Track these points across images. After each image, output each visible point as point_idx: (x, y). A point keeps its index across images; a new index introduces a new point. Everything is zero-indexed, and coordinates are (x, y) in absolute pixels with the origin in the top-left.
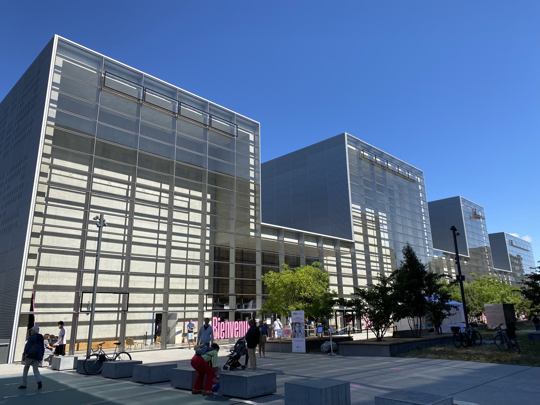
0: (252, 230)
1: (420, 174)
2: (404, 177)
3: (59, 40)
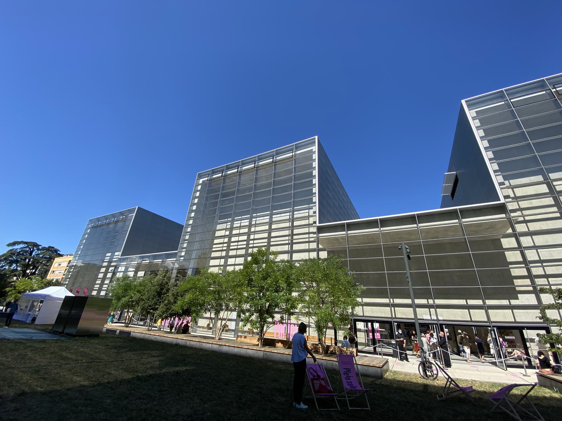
3: (466, 102)
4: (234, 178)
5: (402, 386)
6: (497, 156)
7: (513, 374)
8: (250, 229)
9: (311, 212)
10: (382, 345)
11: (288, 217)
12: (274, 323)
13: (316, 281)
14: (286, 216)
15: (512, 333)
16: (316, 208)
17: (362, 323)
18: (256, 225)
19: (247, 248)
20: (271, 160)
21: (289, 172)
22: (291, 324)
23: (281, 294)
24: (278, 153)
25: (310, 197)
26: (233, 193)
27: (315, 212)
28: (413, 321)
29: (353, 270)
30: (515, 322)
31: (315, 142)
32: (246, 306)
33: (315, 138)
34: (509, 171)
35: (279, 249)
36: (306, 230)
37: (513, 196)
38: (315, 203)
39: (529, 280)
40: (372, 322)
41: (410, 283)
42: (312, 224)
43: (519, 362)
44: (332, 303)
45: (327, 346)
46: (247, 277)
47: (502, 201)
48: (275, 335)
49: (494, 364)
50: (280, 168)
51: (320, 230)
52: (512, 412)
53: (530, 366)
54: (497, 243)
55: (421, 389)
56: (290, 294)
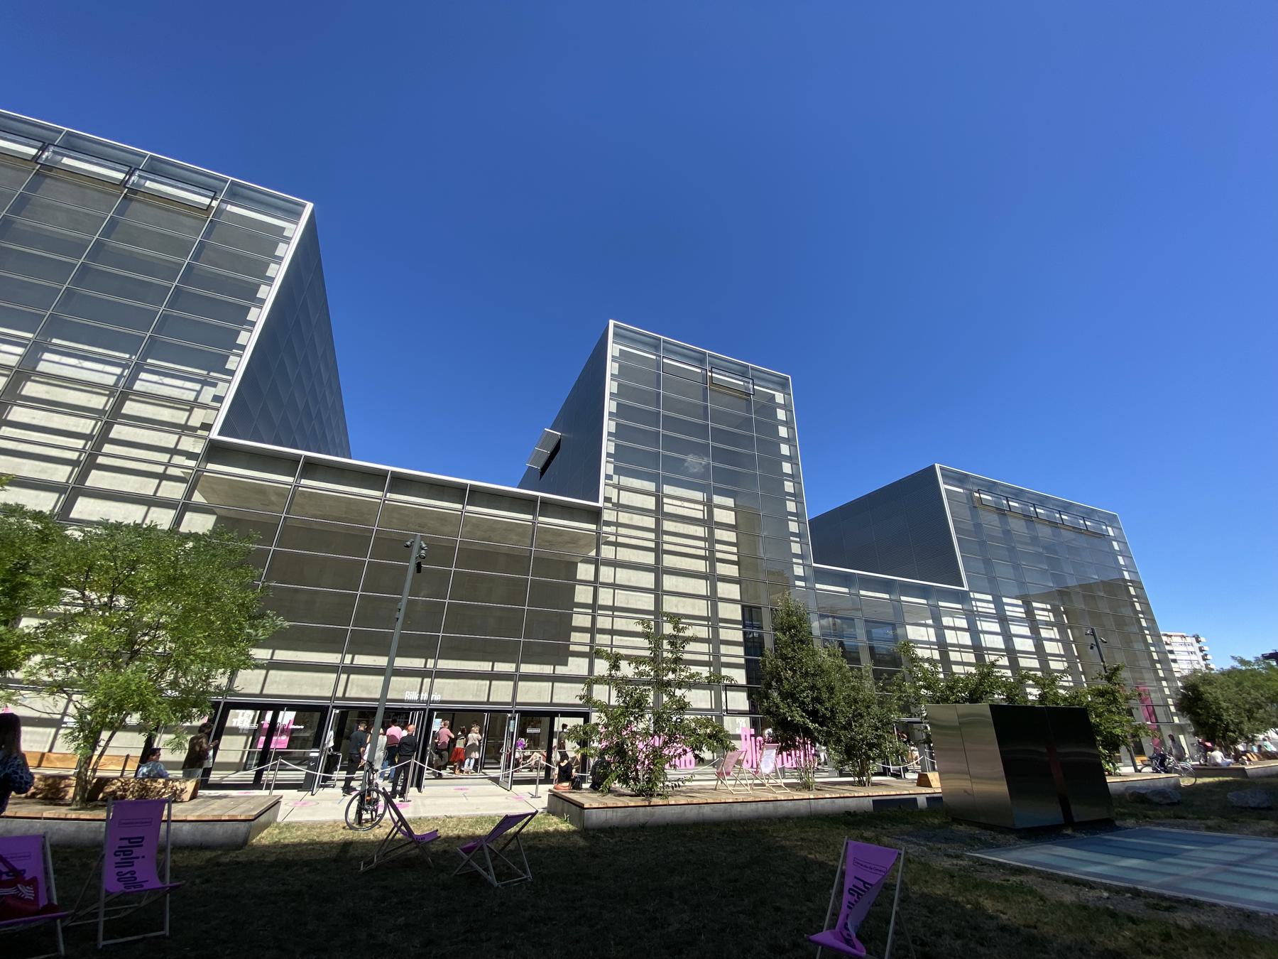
0: (799, 578)
1: (1112, 520)
2: (1076, 530)
3: (615, 326)
5: (290, 856)
6: (619, 433)
9: (208, 394)
10: (282, 764)
11: (110, 380)
13: (130, 593)
14: (108, 375)
16: (229, 391)
17: (250, 713)
20: (121, 176)
24: (155, 170)
25: (224, 352)
29: (271, 574)
31: (299, 215)
33: (304, 206)
34: (628, 462)
36: (169, 440)
38: (232, 373)
42: (194, 429)
43: (534, 774)
44: (166, 658)
47: (600, 504)
49: (495, 780)
50: (138, 217)
52: (486, 869)
53: (547, 780)
54: (574, 566)
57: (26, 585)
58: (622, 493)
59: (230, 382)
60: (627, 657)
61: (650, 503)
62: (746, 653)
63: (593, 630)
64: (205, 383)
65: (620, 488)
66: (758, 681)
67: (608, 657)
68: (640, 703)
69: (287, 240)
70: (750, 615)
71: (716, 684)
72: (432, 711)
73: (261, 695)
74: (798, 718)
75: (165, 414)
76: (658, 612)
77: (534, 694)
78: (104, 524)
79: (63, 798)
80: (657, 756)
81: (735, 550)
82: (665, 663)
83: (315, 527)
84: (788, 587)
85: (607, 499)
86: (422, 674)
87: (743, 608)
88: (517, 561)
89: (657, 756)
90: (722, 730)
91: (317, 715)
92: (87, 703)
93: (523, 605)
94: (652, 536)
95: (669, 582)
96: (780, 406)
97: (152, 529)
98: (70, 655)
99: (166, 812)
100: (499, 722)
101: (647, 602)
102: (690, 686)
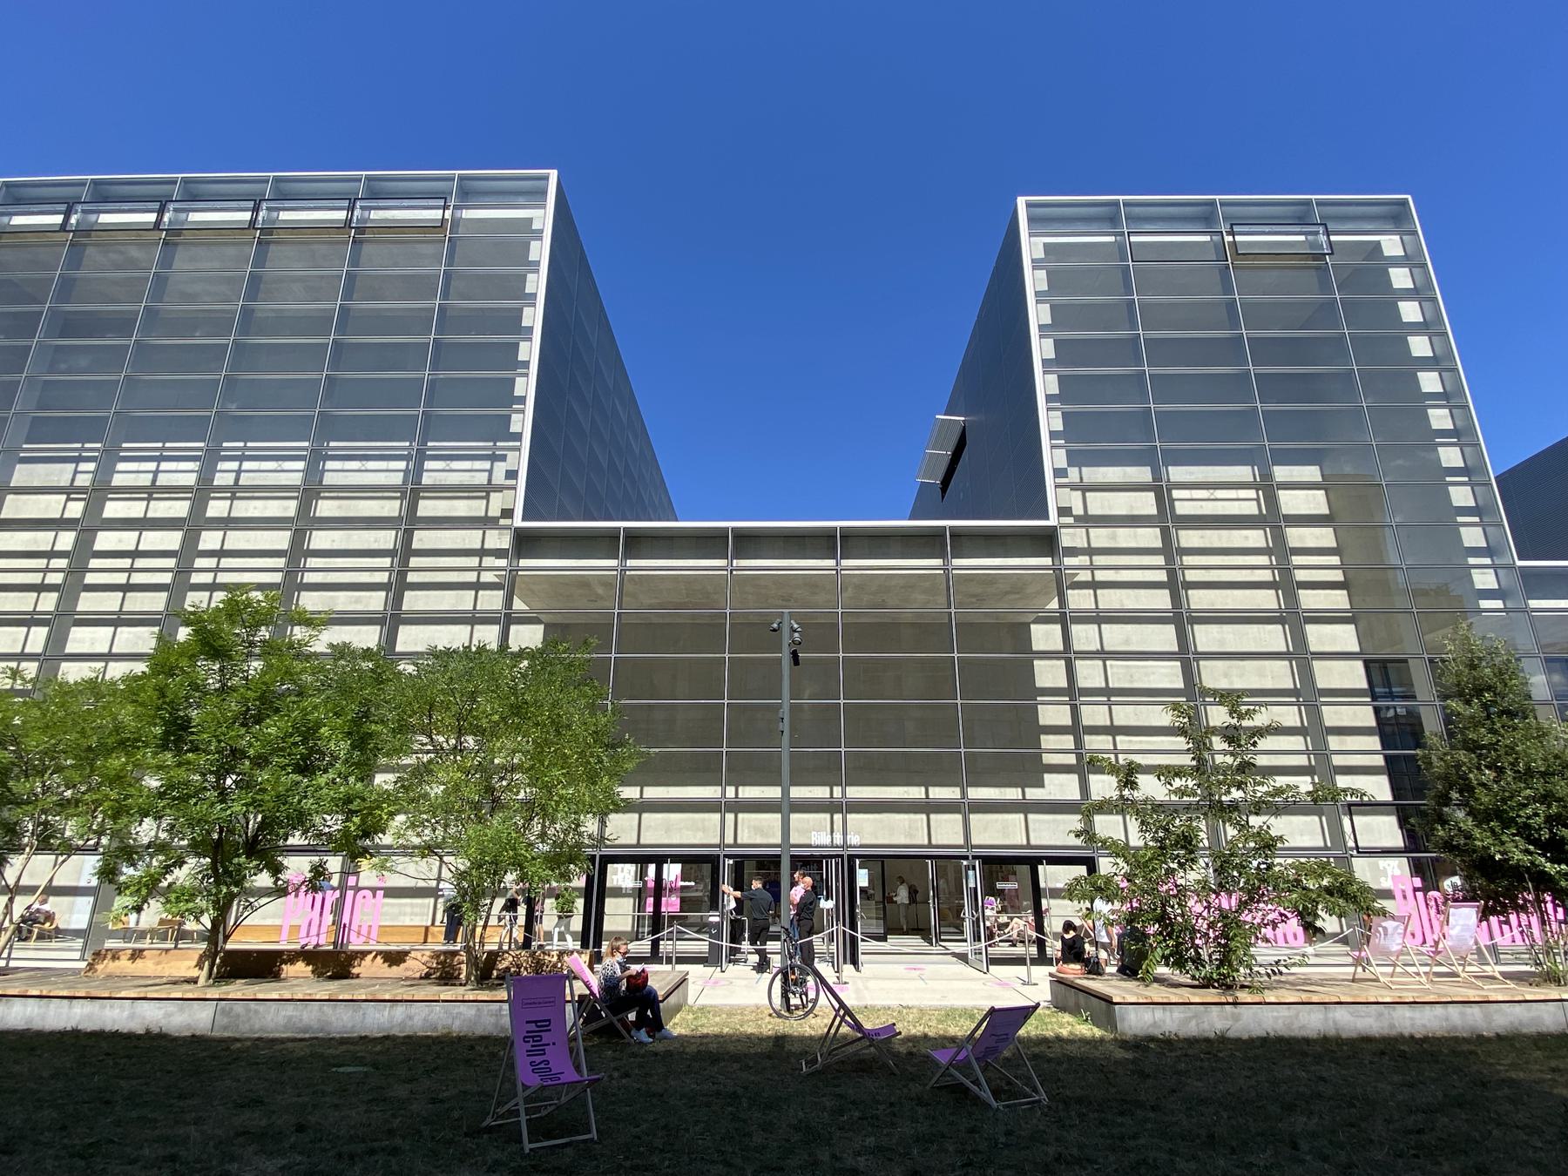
3: (1029, 205)
4: (134, 252)
5: (713, 1047)
6: (1068, 391)
7: (1002, 984)
8: (199, 505)
9: (500, 469)
10: (679, 932)
11: (397, 479)
12: (280, 892)
13: (477, 731)
14: (391, 473)
15: (1015, 873)
16: (520, 460)
17: (631, 868)
18: (235, 492)
19: (180, 585)
20: (342, 215)
21: (419, 286)
22: (357, 889)
23: (322, 780)
26: (123, 325)
27: (511, 474)
28: (777, 851)
29: (615, 695)
30: (1029, 846)
31: (544, 193)
32: (146, 831)
33: (546, 178)
35: (343, 601)
36: (471, 539)
37: (1081, 512)
39: (1071, 738)
40: (659, 860)
41: (786, 739)
42: (495, 520)
43: (1019, 950)
44: (529, 806)
45: (490, 953)
46: (165, 711)
47: (1053, 521)
48: (285, 935)
49: (963, 957)
50: (379, 262)
51: (526, 543)
52: (976, 1082)
53: (1042, 959)
54: (1020, 634)
55: (766, 1047)
56: (366, 778)
57: (370, 735)
58: (1091, 496)
59: (518, 449)
60: (1148, 770)
61: (1146, 504)
62: (1385, 745)
63: (1076, 729)
64: (494, 458)
65: (1085, 488)
66: (1419, 792)
67: (1113, 770)
68: (1187, 841)
69: (538, 235)
70: (1384, 676)
71: (1326, 802)
72: (852, 858)
73: (638, 845)
74: (1518, 856)
75: (461, 508)
76: (1193, 688)
77: (999, 833)
78: (434, 653)
79: (457, 978)
80: (1229, 926)
81: (1335, 560)
82: (1221, 775)
83: (655, 620)
84: (1465, 613)
85: (1064, 511)
86: (830, 807)
87: (1368, 665)
88: (931, 632)
89: (1229, 926)
90: (1351, 880)
91: (707, 868)
92: (462, 864)
93: (962, 697)
94: (1159, 560)
95: (1206, 637)
96: (1396, 262)
97: (482, 649)
98: (433, 811)
99: (568, 991)
100: (951, 875)
101: (1168, 675)
102: (1277, 811)
